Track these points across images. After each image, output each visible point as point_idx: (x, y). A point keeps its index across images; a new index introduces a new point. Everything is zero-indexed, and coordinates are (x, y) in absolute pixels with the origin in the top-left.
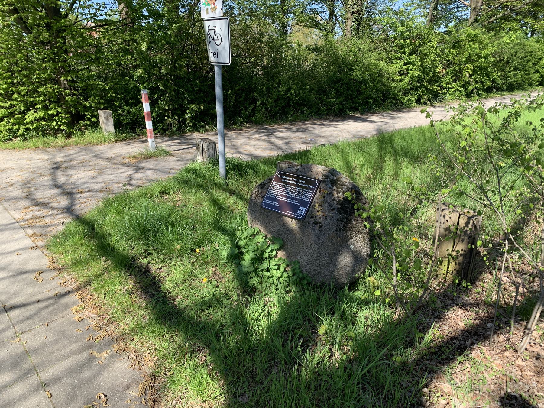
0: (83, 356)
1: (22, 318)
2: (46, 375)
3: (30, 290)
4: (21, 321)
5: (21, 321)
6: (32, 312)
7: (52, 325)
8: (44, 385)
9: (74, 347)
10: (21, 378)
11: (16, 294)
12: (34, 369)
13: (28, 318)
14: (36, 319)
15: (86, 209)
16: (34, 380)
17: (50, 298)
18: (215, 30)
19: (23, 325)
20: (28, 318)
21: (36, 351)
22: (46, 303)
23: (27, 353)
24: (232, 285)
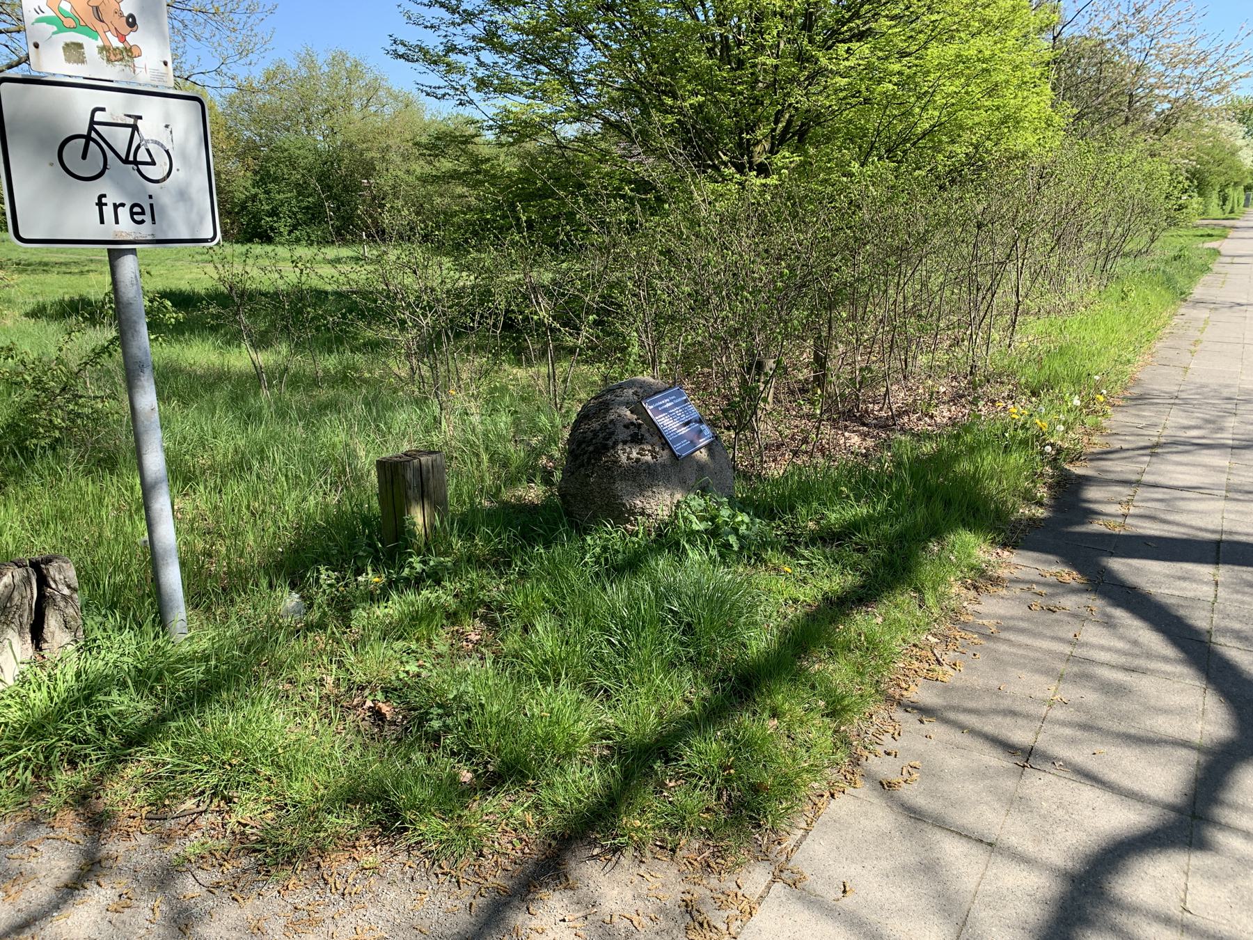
0: (1003, 635)
1: (1020, 721)
2: (1067, 649)
3: (953, 761)
4: (1027, 716)
5: (1027, 716)
6: (999, 719)
7: (994, 683)
8: (1072, 643)
9: (1003, 647)
10: (1091, 661)
11: (981, 774)
12: (1069, 659)
13: (1013, 713)
14: (1006, 703)
15: (17, 863)
16: (1078, 652)
17: (946, 721)
18: (135, 128)
19: (1031, 709)
20: (1013, 713)
21: (1047, 672)
22: (963, 718)
23: (1061, 678)
24: (843, 662)
